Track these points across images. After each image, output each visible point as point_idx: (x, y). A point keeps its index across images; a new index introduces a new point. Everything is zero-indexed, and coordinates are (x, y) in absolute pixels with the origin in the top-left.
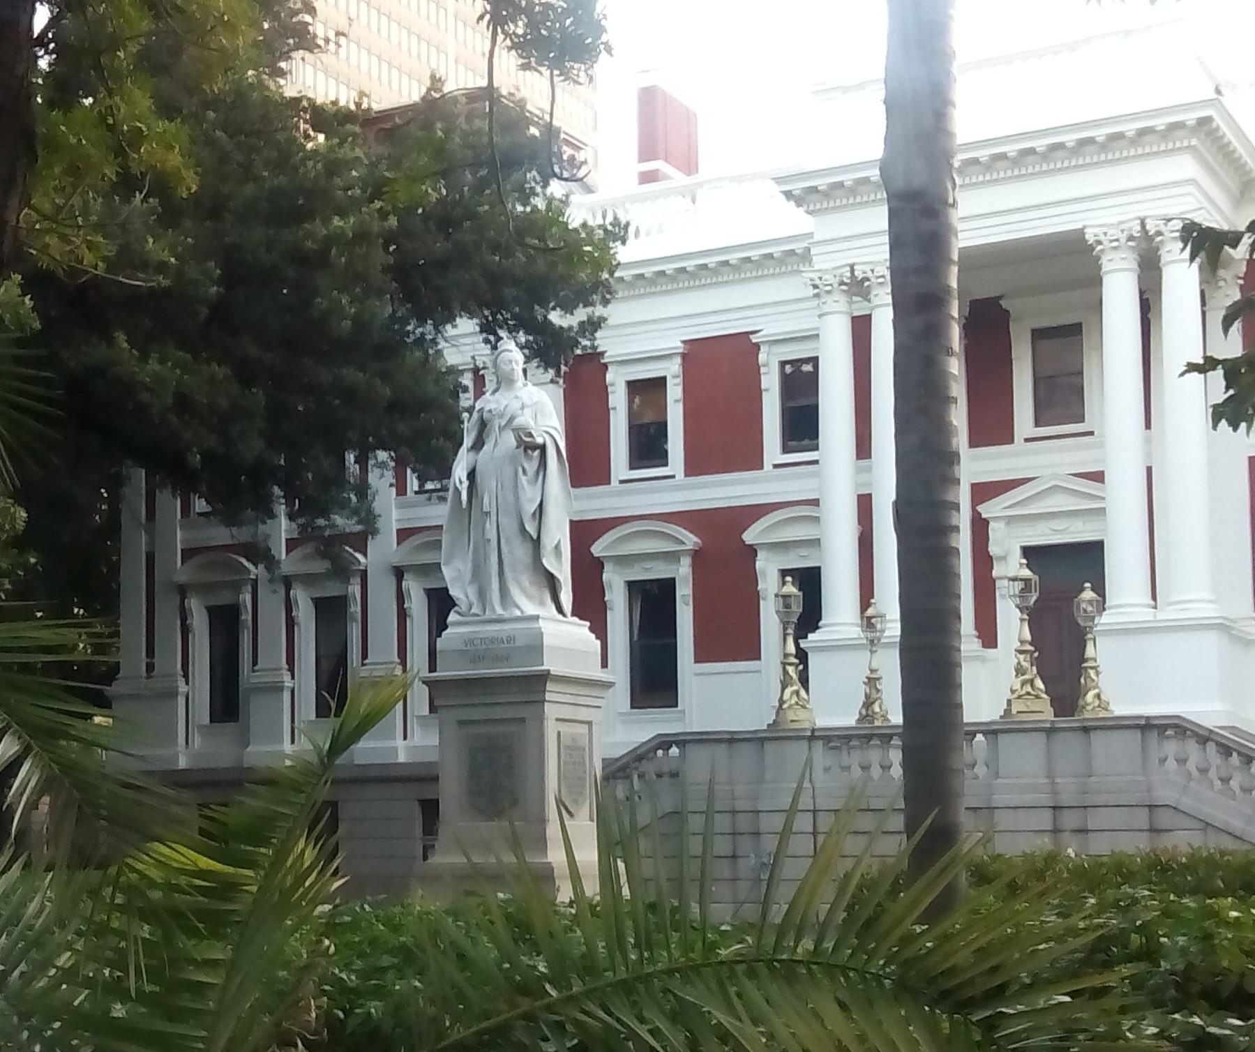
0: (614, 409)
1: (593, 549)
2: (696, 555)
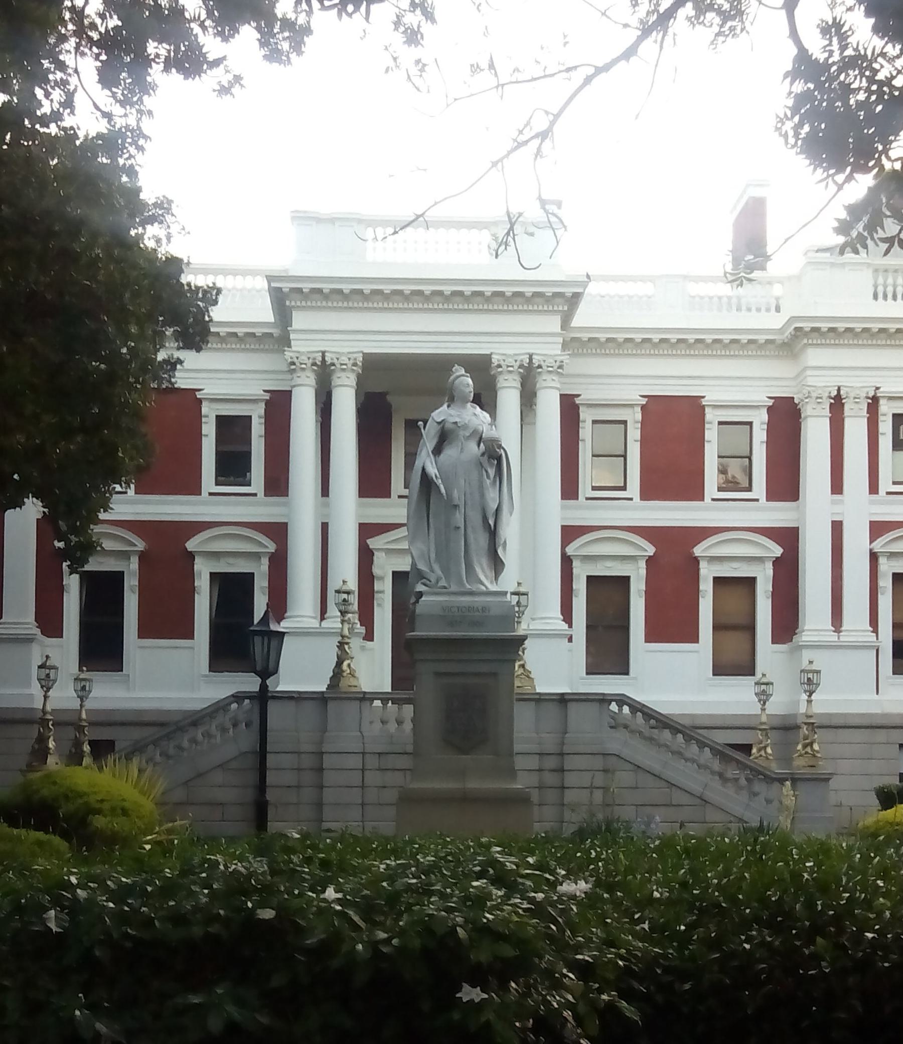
0: (583, 440)
1: (186, 545)
2: (650, 561)
